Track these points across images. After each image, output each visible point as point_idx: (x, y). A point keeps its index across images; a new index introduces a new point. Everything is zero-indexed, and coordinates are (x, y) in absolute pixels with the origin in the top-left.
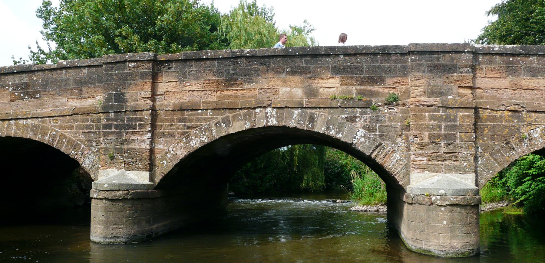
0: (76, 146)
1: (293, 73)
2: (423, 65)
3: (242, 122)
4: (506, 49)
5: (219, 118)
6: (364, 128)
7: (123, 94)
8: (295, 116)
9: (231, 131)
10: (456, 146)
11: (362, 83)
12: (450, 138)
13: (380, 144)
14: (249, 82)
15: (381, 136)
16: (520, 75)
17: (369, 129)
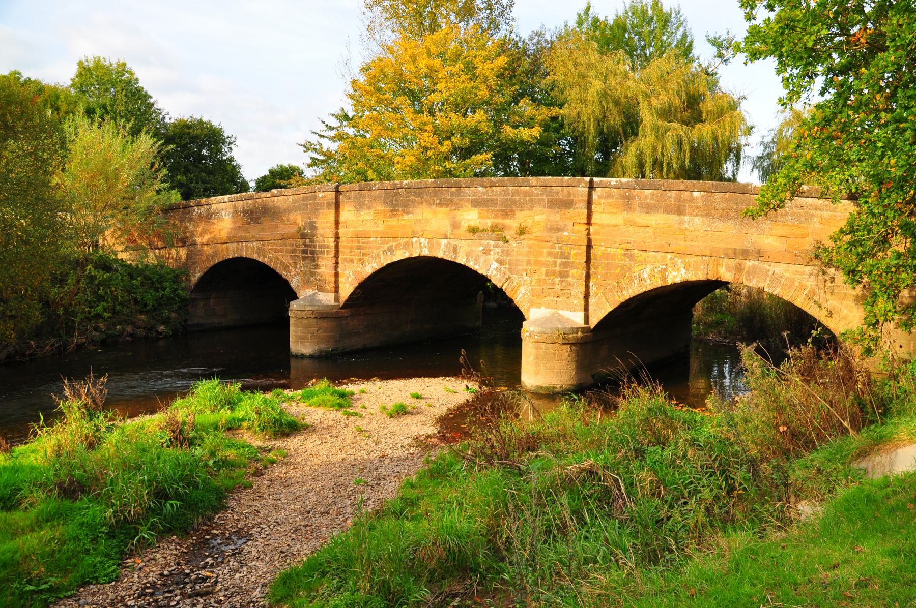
0: (286, 268)
1: (441, 205)
2: (543, 200)
3: (402, 251)
4: (621, 183)
5: (386, 246)
6: (497, 261)
7: (315, 222)
8: (442, 247)
9: (395, 259)
10: (569, 284)
11: (496, 216)
12: (563, 275)
13: (509, 277)
14: (408, 213)
15: (510, 270)
16: (634, 211)
17: (501, 262)
